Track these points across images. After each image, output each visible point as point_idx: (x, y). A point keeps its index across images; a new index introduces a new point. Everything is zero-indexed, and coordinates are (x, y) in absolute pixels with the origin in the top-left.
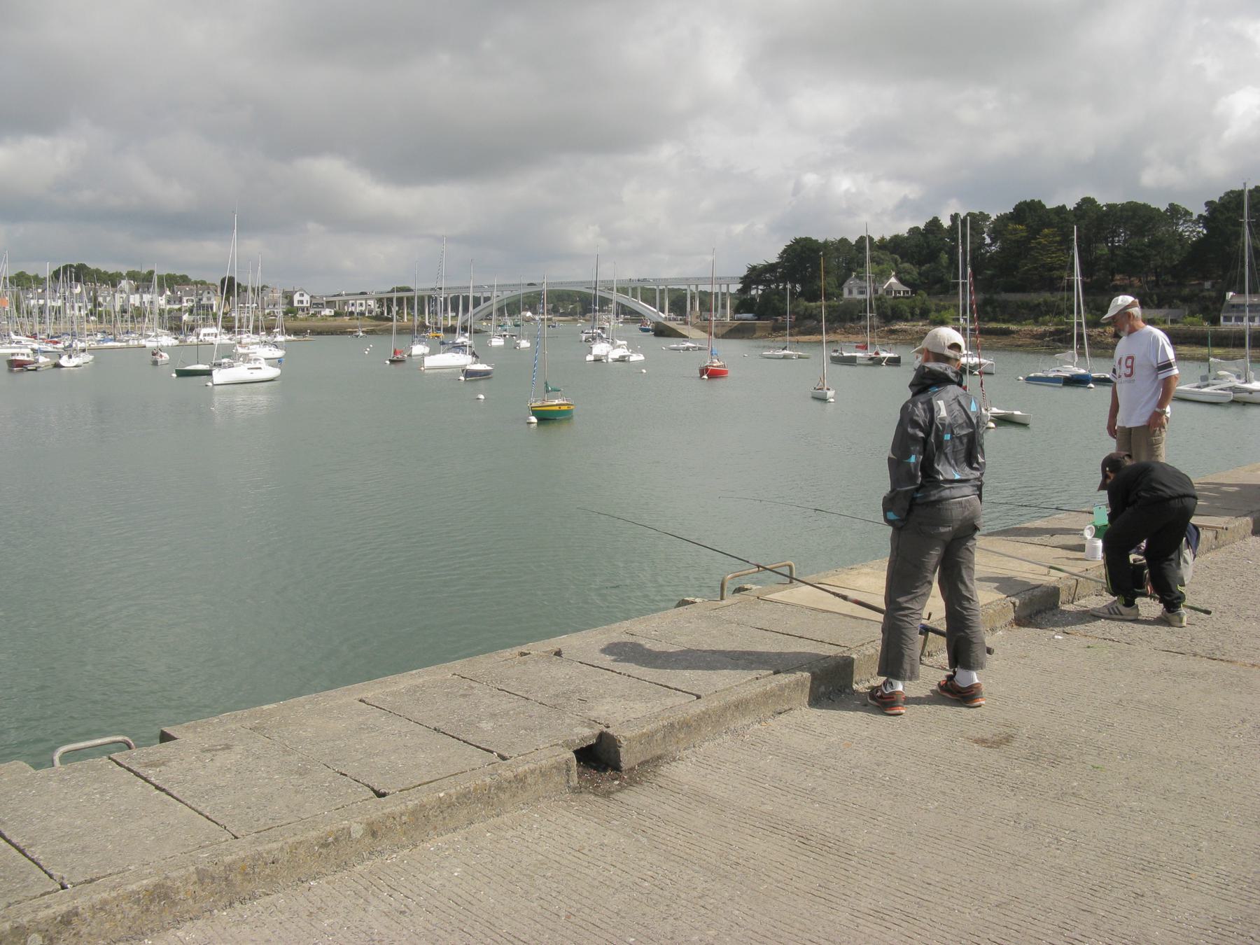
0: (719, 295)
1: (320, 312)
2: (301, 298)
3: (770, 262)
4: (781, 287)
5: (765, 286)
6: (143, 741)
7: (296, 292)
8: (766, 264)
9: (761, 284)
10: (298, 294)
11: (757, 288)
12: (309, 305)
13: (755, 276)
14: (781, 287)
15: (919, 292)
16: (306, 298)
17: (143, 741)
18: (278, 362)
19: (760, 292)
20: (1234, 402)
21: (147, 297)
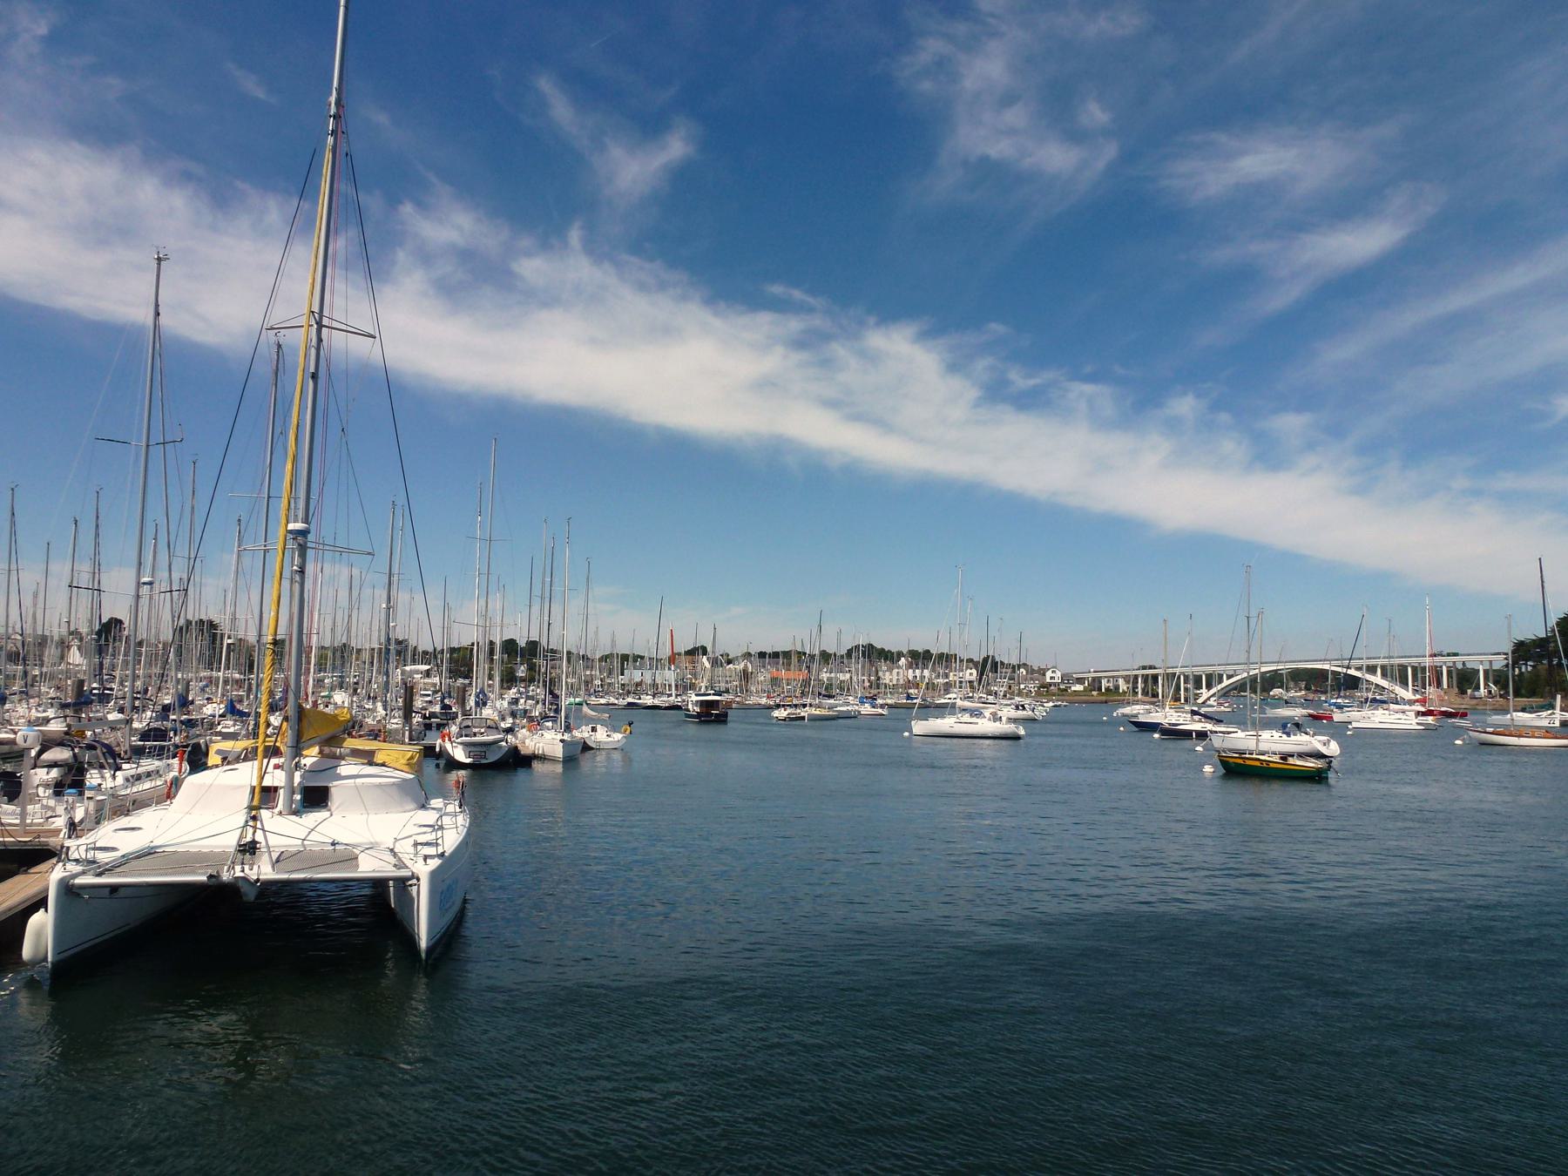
0: (257, 790)
1: (1070, 687)
2: (1053, 675)
3: (1540, 636)
4: (1555, 663)
5: (1534, 662)
6: (1153, 1148)
7: (1049, 669)
8: (1534, 638)
9: (1530, 660)
10: (1050, 671)
11: (1526, 665)
12: (1060, 681)
13: (1522, 650)
14: (1555, 663)
15: (304, 753)
16: (1059, 674)
17: (1153, 1148)
18: (412, 999)
19: (1530, 669)
20: (138, 596)
21: (918, 672)
